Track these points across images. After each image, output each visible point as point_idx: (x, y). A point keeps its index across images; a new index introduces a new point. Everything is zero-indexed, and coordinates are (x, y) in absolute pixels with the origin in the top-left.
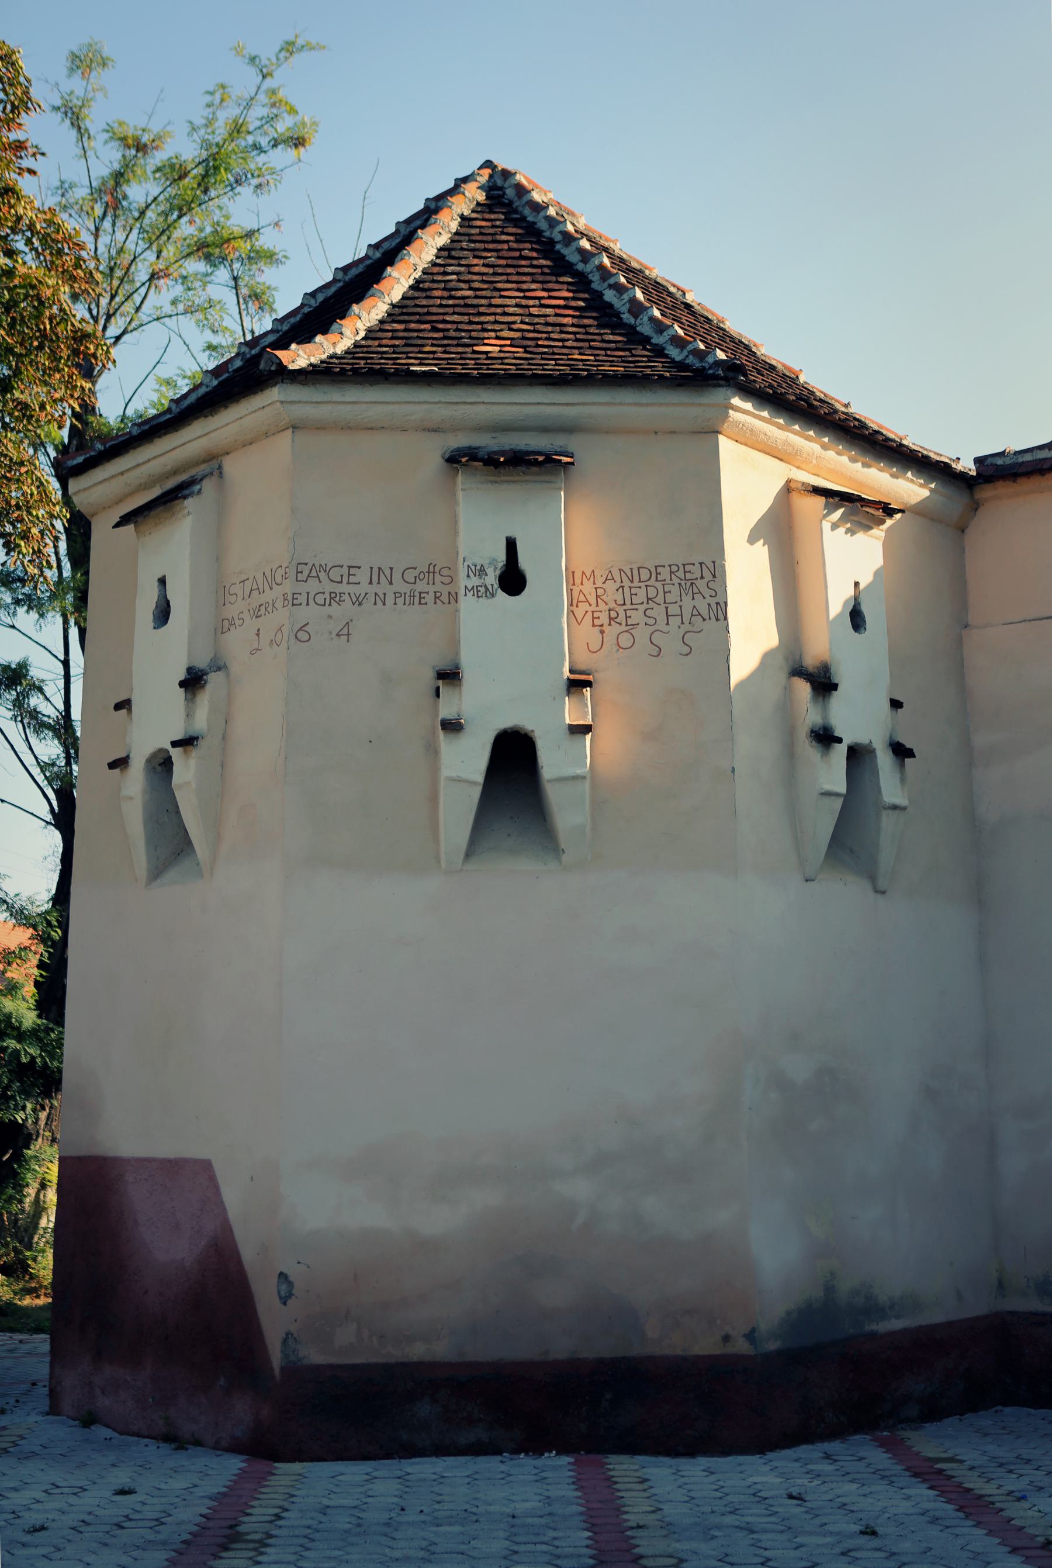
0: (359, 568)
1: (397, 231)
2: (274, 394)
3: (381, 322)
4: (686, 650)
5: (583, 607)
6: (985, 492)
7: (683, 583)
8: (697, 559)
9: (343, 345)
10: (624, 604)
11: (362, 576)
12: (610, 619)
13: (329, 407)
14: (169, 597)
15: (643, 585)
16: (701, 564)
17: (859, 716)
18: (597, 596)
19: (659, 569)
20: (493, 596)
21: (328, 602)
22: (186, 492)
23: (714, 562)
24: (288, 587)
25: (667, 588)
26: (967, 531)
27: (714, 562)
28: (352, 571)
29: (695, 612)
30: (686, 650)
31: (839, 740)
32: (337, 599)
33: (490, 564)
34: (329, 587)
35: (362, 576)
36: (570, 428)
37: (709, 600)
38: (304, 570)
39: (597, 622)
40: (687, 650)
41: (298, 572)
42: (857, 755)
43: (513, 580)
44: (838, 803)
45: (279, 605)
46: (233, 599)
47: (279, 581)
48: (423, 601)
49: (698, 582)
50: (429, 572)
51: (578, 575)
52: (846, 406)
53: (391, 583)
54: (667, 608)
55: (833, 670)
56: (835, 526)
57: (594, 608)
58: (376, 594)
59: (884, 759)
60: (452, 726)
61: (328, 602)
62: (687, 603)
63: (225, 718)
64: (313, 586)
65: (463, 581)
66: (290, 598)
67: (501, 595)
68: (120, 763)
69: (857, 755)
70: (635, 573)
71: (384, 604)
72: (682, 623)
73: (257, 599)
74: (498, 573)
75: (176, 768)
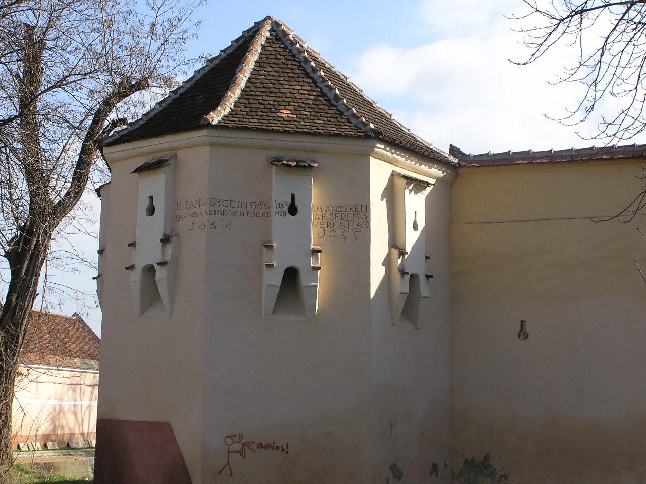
1: (232, 45)
2: (204, 132)
3: (239, 98)
7: (355, 213)
9: (227, 111)
11: (235, 204)
13: (225, 139)
15: (340, 213)
20: (286, 215)
22: (164, 165)
24: (207, 207)
28: (232, 202)
34: (223, 208)
35: (235, 204)
36: (314, 151)
37: (364, 220)
38: (214, 201)
42: (414, 278)
43: (293, 210)
45: (203, 213)
46: (181, 208)
47: (203, 204)
48: (258, 215)
49: (361, 213)
52: (409, 130)
56: (411, 191)
57: (321, 221)
59: (422, 279)
62: (356, 221)
63: (177, 256)
64: (217, 208)
65: (274, 210)
68: (131, 267)
69: (414, 278)
73: (192, 210)
74: (288, 207)
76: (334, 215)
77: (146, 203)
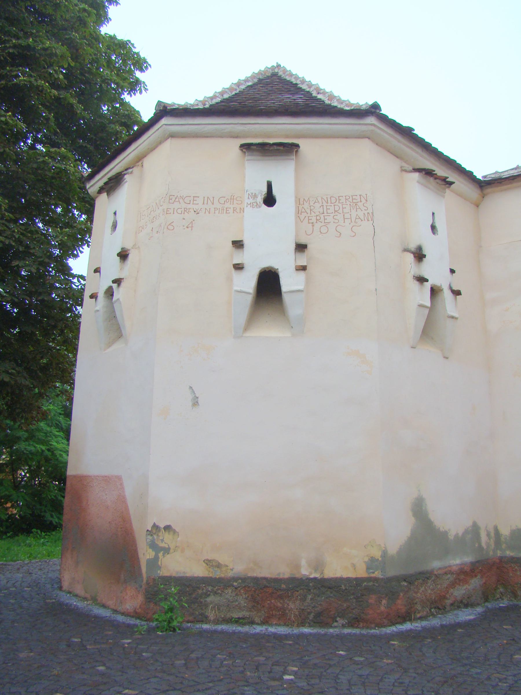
5: (304, 215)
6: (489, 190)
7: (352, 204)
10: (323, 213)
11: (200, 201)
12: (317, 220)
13: (187, 127)
16: (360, 195)
17: (435, 271)
18: (311, 210)
19: (340, 198)
20: (260, 207)
21: (183, 212)
23: (366, 195)
25: (344, 206)
26: (480, 207)
27: (366, 195)
28: (195, 199)
31: (427, 280)
34: (184, 205)
35: (200, 201)
39: (310, 221)
40: (354, 234)
42: (434, 291)
43: (270, 200)
44: (427, 311)
49: (359, 204)
50: (231, 199)
51: (302, 200)
53: (213, 204)
55: (423, 249)
57: (309, 215)
59: (447, 294)
60: (238, 267)
61: (183, 212)
62: (354, 213)
64: (176, 205)
66: (166, 211)
67: (264, 207)
70: (329, 200)
71: (209, 213)
72: (351, 222)
74: (263, 197)
76: (325, 207)
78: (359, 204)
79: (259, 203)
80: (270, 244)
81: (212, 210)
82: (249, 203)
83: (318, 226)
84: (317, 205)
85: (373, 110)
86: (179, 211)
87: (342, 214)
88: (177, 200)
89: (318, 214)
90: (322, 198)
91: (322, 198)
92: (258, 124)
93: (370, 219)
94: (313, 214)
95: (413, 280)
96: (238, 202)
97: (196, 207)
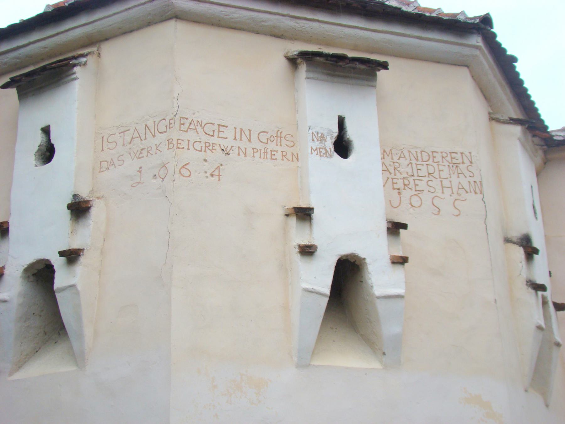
0: (226, 127)
4: (457, 212)
7: (451, 165)
8: (458, 149)
11: (229, 133)
14: (53, 142)
16: (461, 153)
18: (395, 169)
19: (435, 154)
20: (331, 156)
28: (222, 129)
29: (460, 187)
30: (457, 212)
32: (211, 148)
33: (328, 133)
34: (205, 138)
35: (229, 133)
41: (181, 124)
43: (342, 147)
49: (461, 166)
50: (277, 137)
53: (250, 141)
54: (441, 181)
57: (392, 176)
58: (239, 148)
60: (307, 251)
62: (455, 180)
64: (192, 136)
66: (175, 142)
67: (336, 156)
70: (419, 155)
71: (246, 156)
74: (333, 140)
75: (57, 275)
76: (414, 166)
77: (39, 139)
78: (461, 166)
79: (328, 150)
80: (350, 219)
81: (250, 151)
82: (314, 148)
83: (407, 194)
84: (404, 162)
85: (483, 26)
86: (198, 146)
87: (439, 180)
88: (192, 127)
89: (405, 175)
90: (409, 152)
91: (409, 152)
92: (318, 21)
93: (478, 191)
94: (398, 175)
95: (526, 287)
96: (288, 143)
97: (223, 143)
